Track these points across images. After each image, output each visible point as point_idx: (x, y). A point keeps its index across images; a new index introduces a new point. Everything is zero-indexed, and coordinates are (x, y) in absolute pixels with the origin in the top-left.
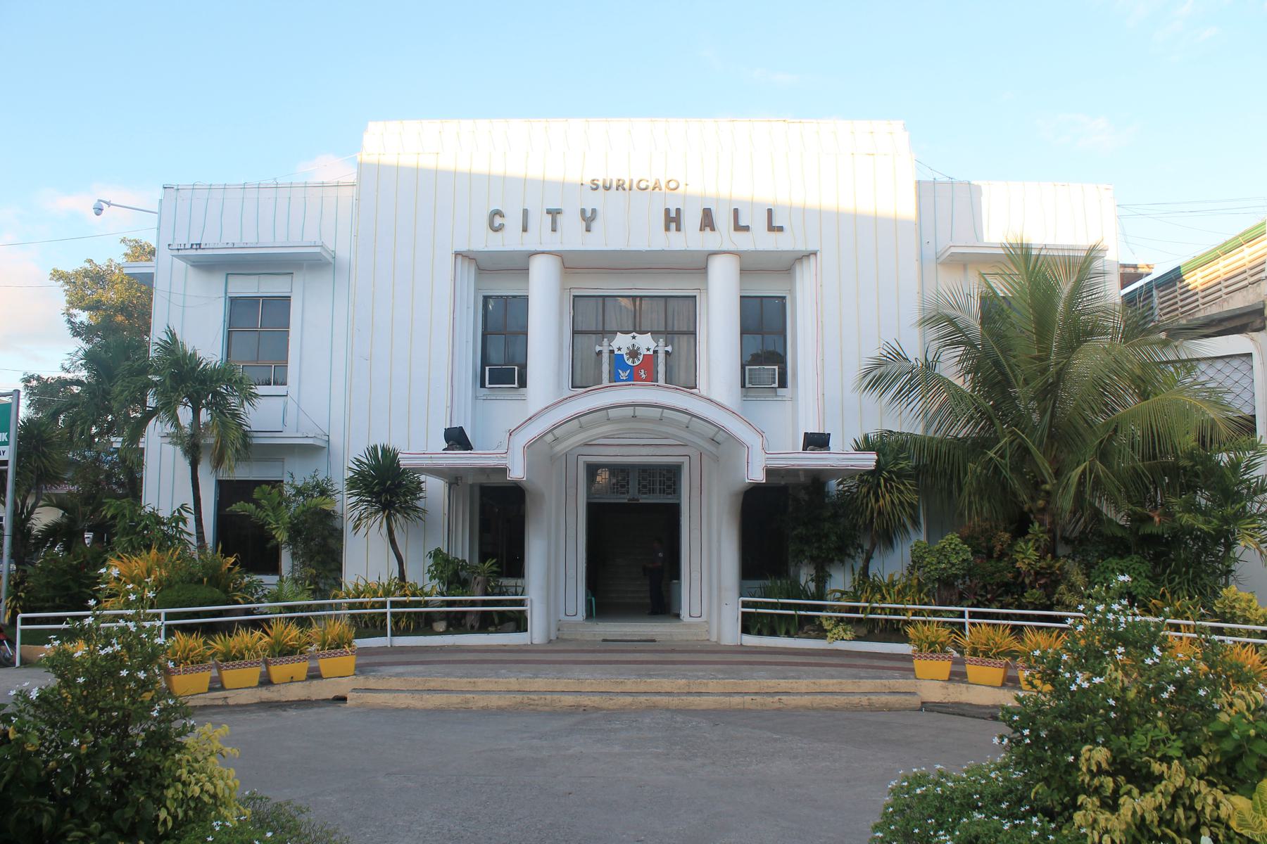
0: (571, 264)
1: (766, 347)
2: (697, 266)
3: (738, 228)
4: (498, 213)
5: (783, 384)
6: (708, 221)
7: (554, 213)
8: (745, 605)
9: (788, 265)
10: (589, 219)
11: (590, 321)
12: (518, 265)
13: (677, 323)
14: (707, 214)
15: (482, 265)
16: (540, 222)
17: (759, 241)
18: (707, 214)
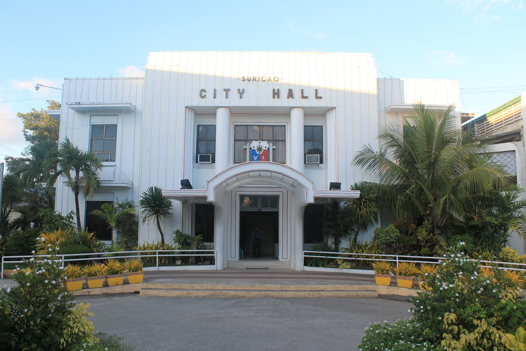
0: (234, 112)
1: (314, 146)
2: (286, 113)
3: (303, 97)
4: (203, 90)
5: (321, 162)
6: (290, 94)
7: (227, 91)
8: (305, 254)
9: (324, 113)
10: (241, 93)
11: (241, 136)
12: (212, 112)
14: (290, 91)
15: (197, 112)
16: (221, 94)
18: (290, 91)
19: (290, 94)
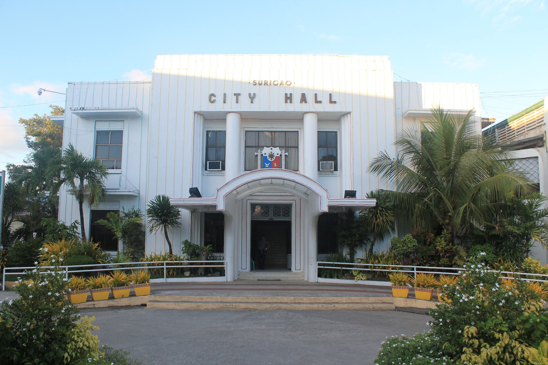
0: (244, 117)
1: (329, 153)
2: (299, 118)
3: (317, 102)
4: (213, 95)
5: (336, 169)
6: (304, 99)
7: (237, 95)
8: (319, 265)
9: (338, 118)
10: (252, 98)
11: (252, 142)
12: (221, 118)
13: (290, 143)
14: (303, 95)
15: (206, 117)
16: (231, 99)
17: (326, 107)
18: (303, 95)
19: (304, 99)
